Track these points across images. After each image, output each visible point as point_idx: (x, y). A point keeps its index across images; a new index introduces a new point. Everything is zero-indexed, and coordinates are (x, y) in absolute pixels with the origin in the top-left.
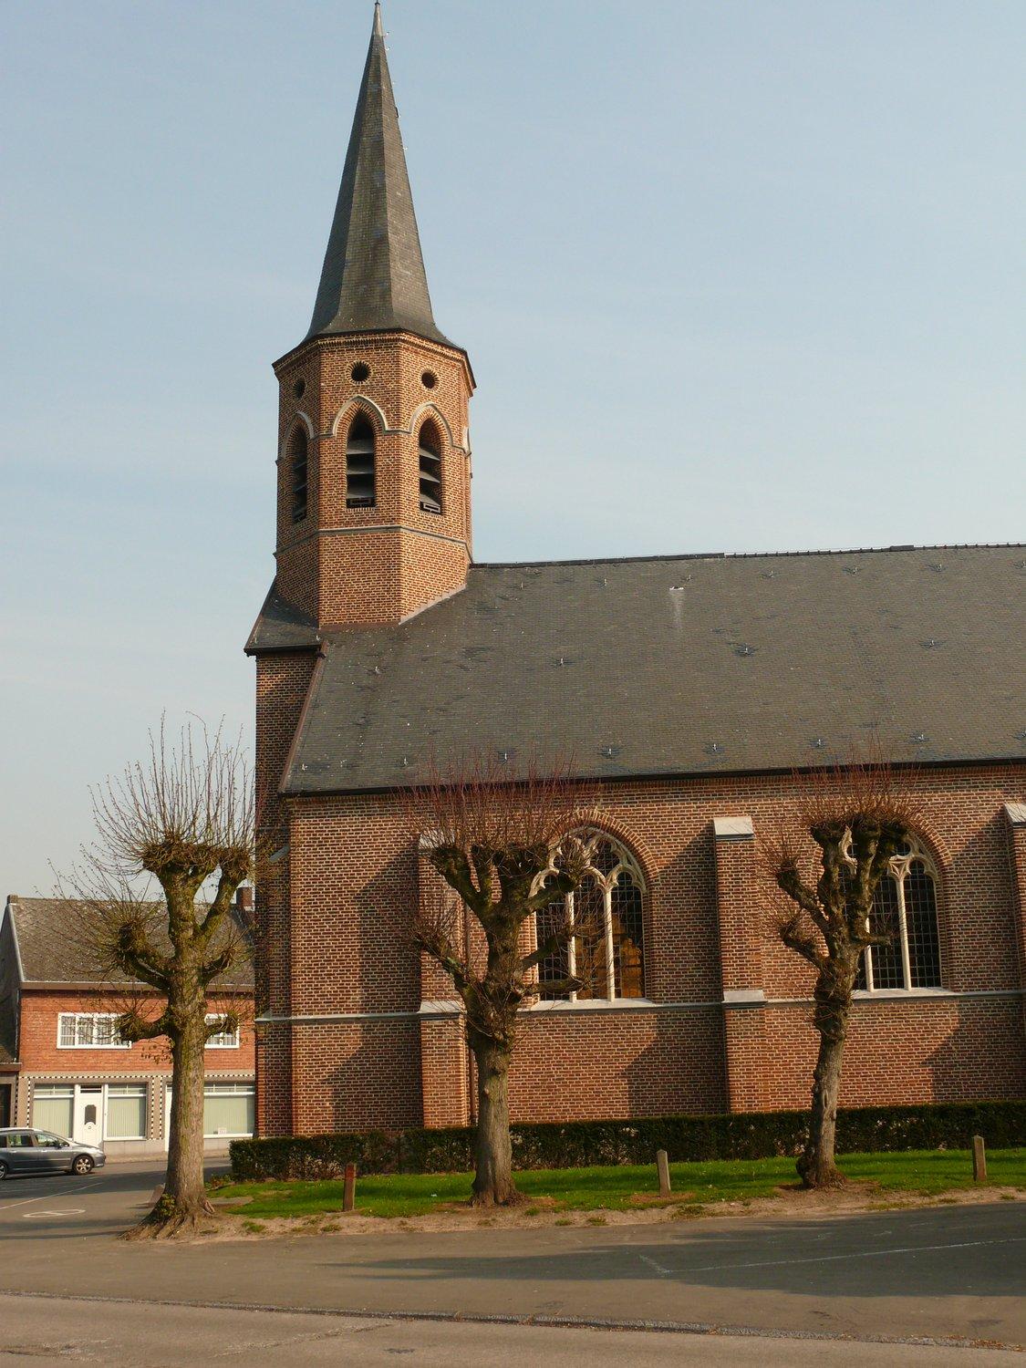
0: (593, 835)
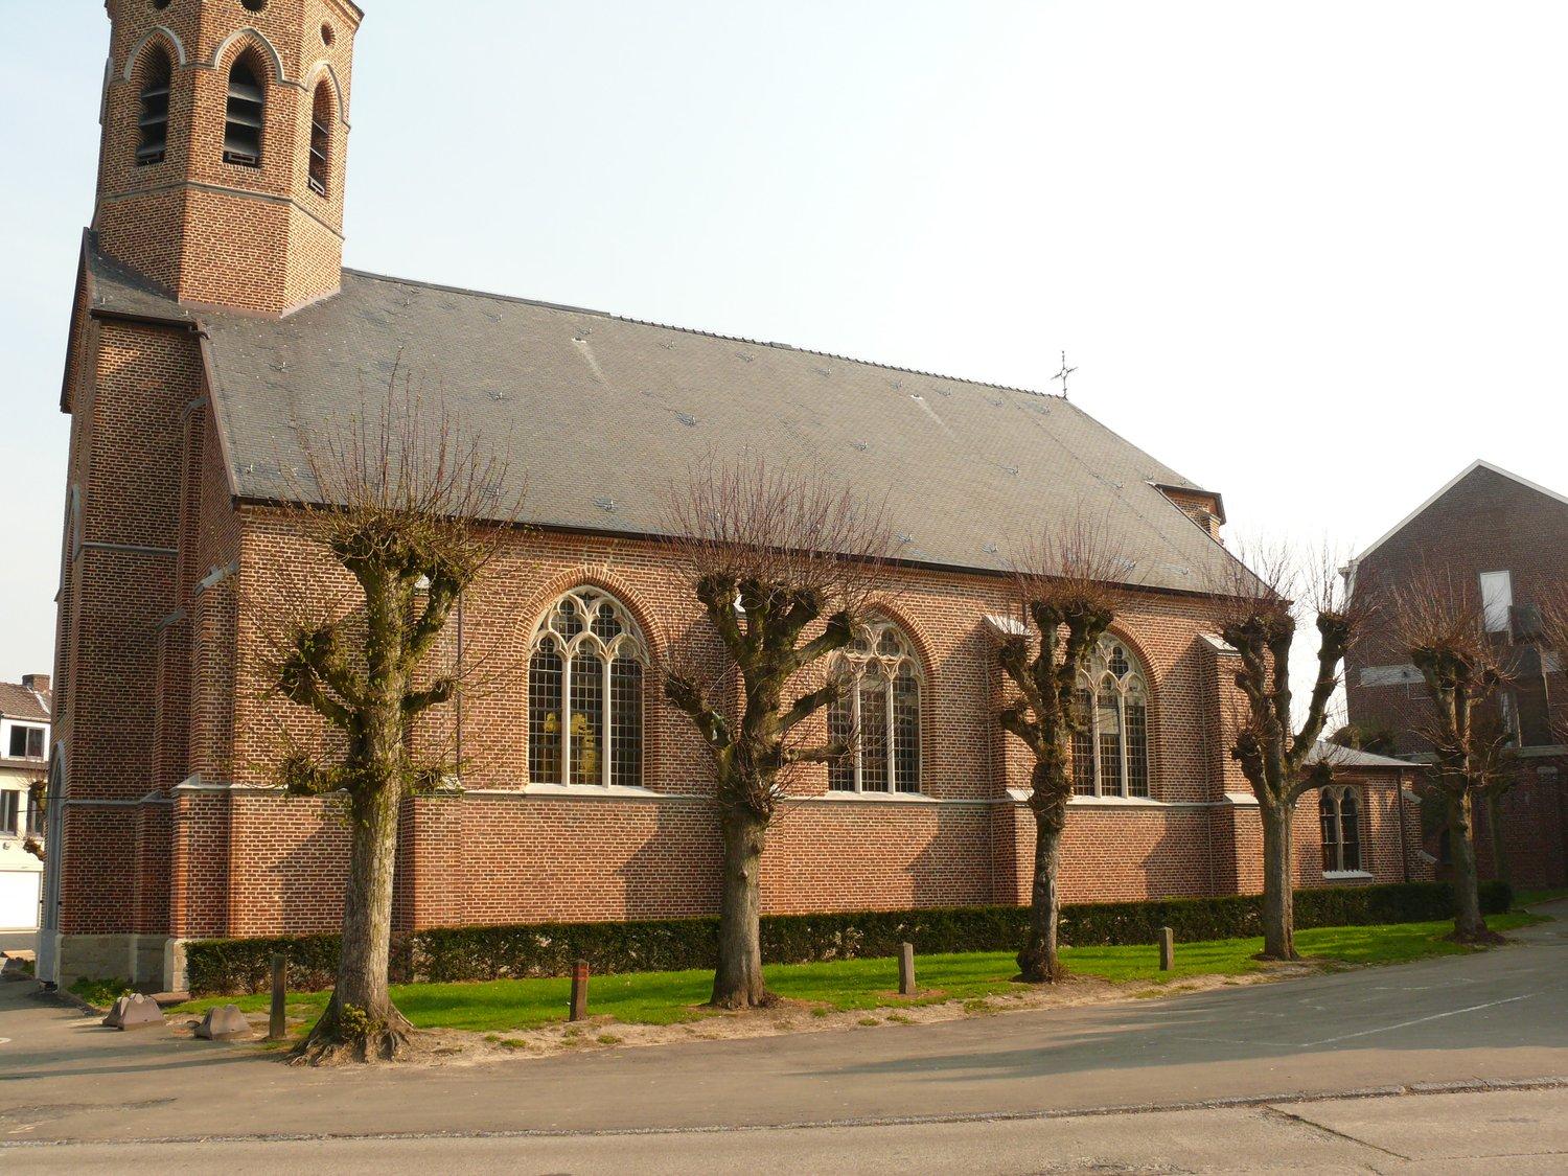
0: (595, 597)
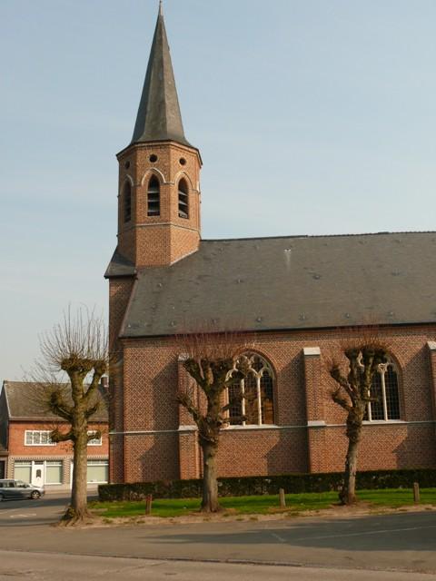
0: (252, 355)
